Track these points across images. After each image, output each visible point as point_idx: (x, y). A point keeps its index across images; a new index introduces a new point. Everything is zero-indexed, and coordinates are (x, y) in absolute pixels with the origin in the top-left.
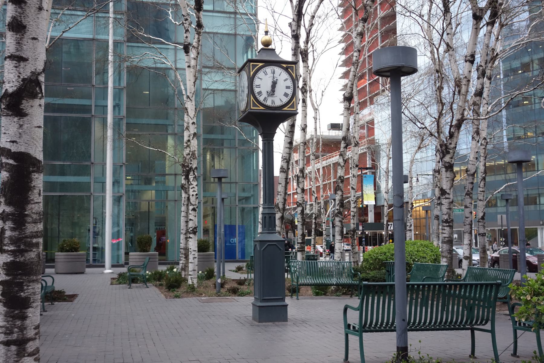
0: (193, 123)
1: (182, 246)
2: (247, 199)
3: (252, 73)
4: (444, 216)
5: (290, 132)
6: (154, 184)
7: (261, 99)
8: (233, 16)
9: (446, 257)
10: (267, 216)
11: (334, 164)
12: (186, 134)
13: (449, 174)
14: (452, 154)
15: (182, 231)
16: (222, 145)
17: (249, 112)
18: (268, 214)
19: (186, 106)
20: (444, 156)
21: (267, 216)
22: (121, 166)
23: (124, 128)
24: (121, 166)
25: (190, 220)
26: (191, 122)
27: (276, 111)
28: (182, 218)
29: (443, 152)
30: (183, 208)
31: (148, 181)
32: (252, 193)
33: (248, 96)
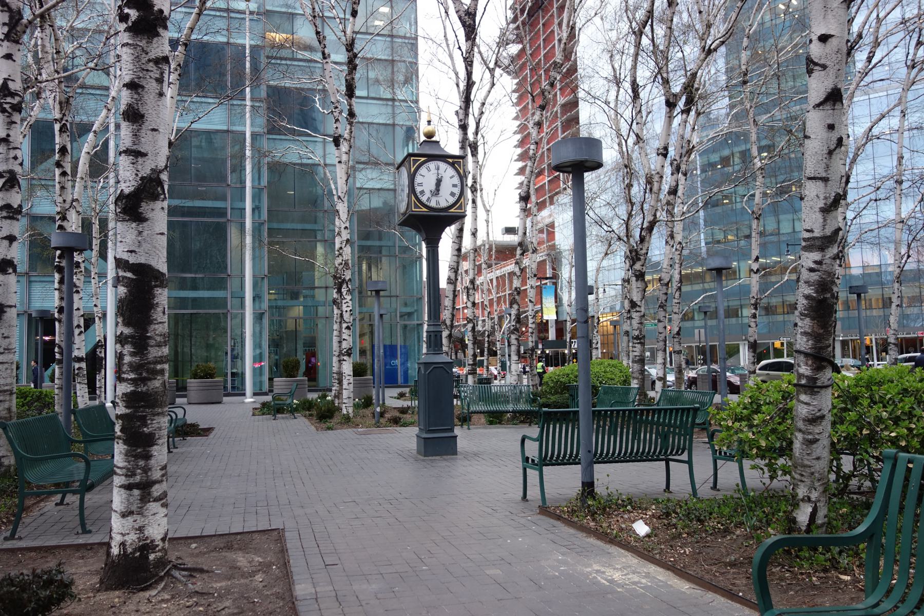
0: (346, 228)
1: (335, 369)
2: (410, 315)
3: (413, 169)
7: (424, 199)
9: (637, 378)
12: (338, 241)
13: (640, 284)
16: (380, 252)
20: (634, 263)
21: (432, 334)
22: (263, 278)
23: (266, 234)
24: (263, 278)
26: (343, 226)
28: (334, 338)
30: (336, 327)
31: (295, 296)
33: (409, 196)
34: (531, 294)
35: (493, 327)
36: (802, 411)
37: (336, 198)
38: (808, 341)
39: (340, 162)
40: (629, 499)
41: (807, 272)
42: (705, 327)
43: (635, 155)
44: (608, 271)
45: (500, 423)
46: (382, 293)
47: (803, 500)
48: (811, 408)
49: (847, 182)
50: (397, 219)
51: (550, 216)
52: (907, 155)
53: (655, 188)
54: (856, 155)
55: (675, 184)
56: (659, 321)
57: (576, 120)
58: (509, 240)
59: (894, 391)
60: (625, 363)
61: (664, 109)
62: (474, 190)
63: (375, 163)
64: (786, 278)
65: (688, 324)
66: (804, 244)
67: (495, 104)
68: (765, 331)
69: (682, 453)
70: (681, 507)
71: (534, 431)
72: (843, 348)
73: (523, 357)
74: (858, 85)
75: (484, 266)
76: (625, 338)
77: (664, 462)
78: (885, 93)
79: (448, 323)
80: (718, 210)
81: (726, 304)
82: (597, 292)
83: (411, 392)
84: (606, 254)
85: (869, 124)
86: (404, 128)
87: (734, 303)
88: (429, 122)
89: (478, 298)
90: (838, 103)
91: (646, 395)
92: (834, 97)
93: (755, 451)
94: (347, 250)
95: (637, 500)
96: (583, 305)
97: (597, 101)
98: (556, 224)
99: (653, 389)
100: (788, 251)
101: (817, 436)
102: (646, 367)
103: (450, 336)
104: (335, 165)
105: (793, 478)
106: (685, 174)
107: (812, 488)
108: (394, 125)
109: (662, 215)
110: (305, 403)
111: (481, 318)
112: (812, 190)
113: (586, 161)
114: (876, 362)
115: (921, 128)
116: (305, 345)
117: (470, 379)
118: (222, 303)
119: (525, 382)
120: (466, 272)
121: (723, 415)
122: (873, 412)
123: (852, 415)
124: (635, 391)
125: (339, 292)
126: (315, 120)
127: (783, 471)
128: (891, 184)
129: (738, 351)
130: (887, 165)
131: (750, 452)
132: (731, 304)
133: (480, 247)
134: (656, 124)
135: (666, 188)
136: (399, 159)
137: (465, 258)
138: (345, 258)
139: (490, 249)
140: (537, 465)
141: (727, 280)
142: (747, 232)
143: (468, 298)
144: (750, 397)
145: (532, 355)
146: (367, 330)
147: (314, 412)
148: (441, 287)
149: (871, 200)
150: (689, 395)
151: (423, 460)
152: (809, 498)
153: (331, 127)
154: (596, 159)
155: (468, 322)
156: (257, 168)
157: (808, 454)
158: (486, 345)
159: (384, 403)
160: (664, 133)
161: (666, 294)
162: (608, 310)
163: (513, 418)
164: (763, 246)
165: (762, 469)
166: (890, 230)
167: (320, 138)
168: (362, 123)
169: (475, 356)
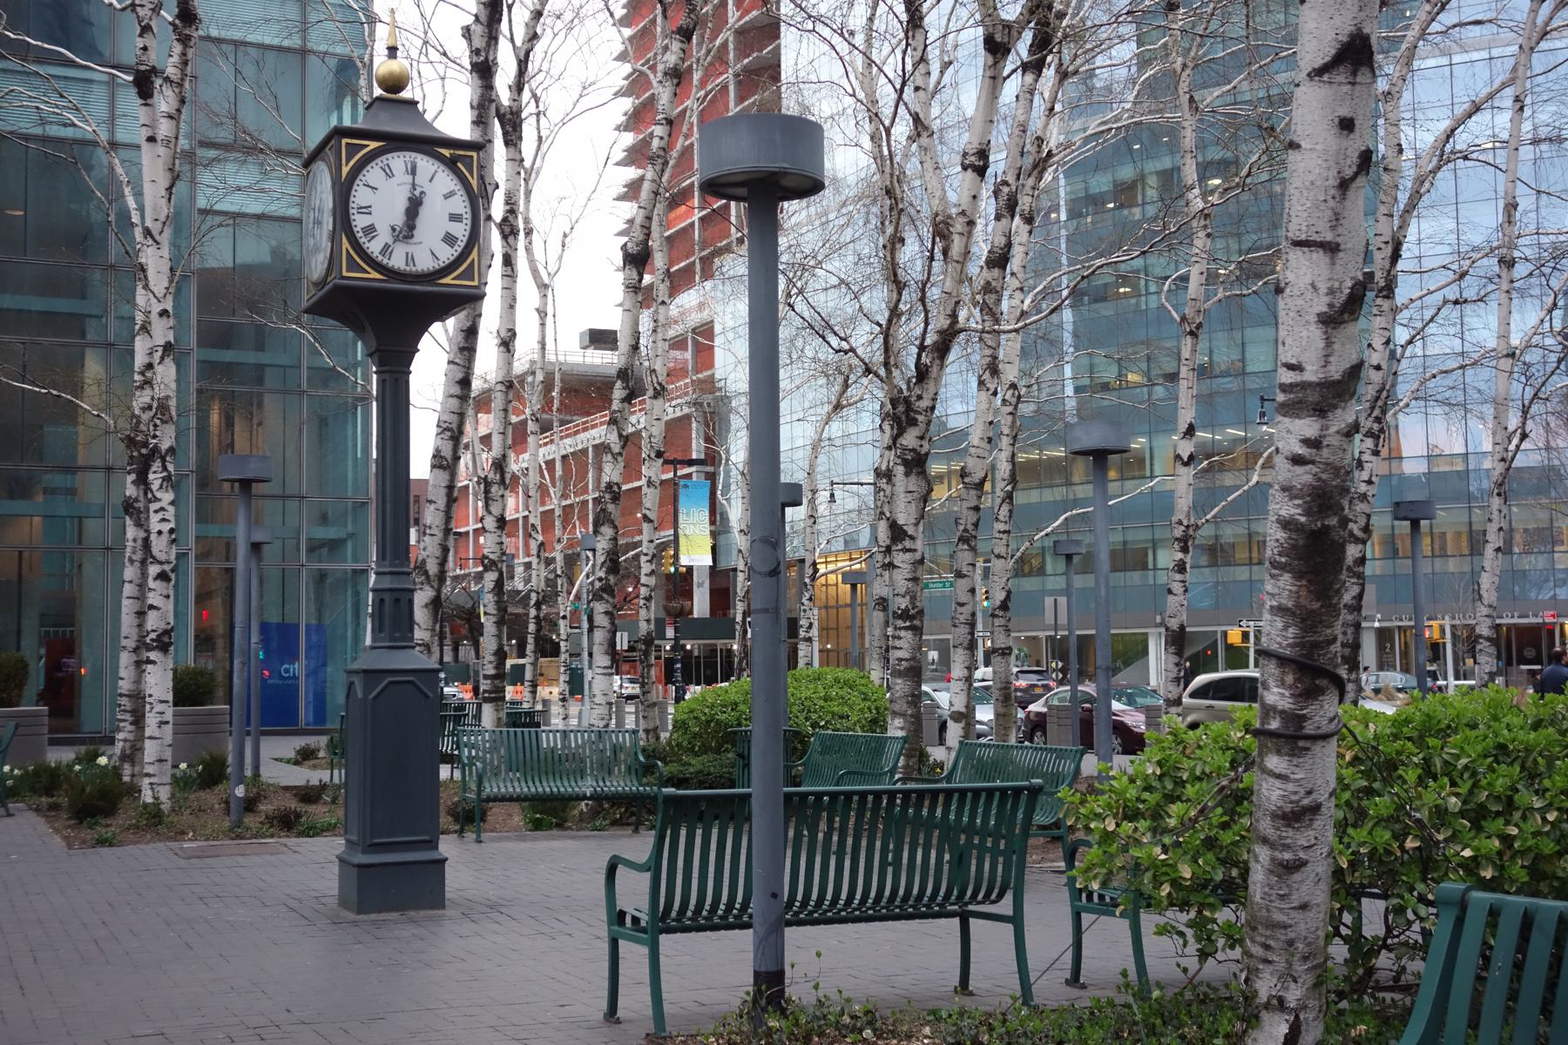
0: (164, 313)
1: (125, 686)
2: (335, 546)
3: (345, 170)
4: (899, 599)
5: (462, 349)
6: (40, 498)
7: (374, 248)
9: (903, 715)
10: (387, 597)
12: (141, 346)
13: (914, 483)
14: (922, 426)
15: (124, 642)
16: (260, 381)
17: (337, 288)
21: (387, 597)
26: (156, 308)
27: (418, 288)
28: (125, 602)
32: (350, 528)
33: (334, 237)
34: (650, 498)
35: (551, 583)
36: (1271, 794)
37: (138, 233)
38: (1286, 628)
39: (151, 139)
40: (867, 1012)
41: (1288, 466)
42: (1067, 592)
43: (912, 167)
44: (833, 447)
45: (560, 826)
46: (257, 488)
47: (1267, 1006)
48: (1291, 787)
49: (1396, 256)
50: (306, 298)
51: (701, 306)
52: (1526, 202)
53: (956, 249)
54: (1416, 196)
55: (1003, 241)
56: (959, 575)
57: (770, 71)
58: (598, 361)
59: (1474, 751)
60: (875, 676)
61: (982, 57)
62: (509, 231)
63: (248, 148)
64: (1255, 479)
65: (1030, 584)
66: (1281, 397)
67: (568, 16)
68: (1206, 603)
69: (1001, 896)
70: (991, 1029)
71: (639, 846)
72: (1381, 648)
73: (627, 660)
74: (1423, 34)
75: (532, 426)
76: (878, 616)
77: (956, 921)
78: (1485, 55)
79: (432, 568)
80: (1106, 309)
81: (1117, 537)
82: (812, 501)
83: (332, 746)
84: (838, 407)
85: (1445, 124)
86: (332, 62)
87: (1138, 536)
88: (392, 51)
89: (513, 507)
90: (1364, 70)
91: (923, 756)
92: (1355, 55)
93: (1166, 889)
94: (166, 373)
95: (887, 1013)
96: (768, 532)
97: (820, 27)
98: (718, 328)
99: (942, 742)
100: (1263, 415)
101: (1302, 855)
102: (925, 688)
103: (436, 604)
104: (138, 147)
105: (1247, 953)
106: (1029, 220)
107: (1289, 976)
108: (303, 52)
109: (970, 316)
110: (36, 773)
111: (522, 559)
112: (1304, 275)
113: (783, 173)
114: (1452, 682)
115: (1559, 140)
117: (488, 715)
119: (630, 722)
120: (486, 440)
121: (1096, 805)
122: (1430, 797)
123: (1381, 805)
124: (897, 747)
125: (142, 481)
126: (91, 24)
127: (1229, 937)
128: (1491, 265)
129: (1145, 652)
130: (1483, 223)
131: (1154, 893)
132: (1130, 536)
133: (522, 379)
134: (963, 94)
135: (981, 249)
136: (315, 138)
137: (483, 403)
138: (159, 392)
139: (548, 385)
140: (644, 931)
141: (1122, 479)
142: (1170, 368)
143: (487, 506)
144: (1159, 763)
145: (646, 653)
146: (219, 585)
147: (64, 801)
148: (413, 476)
149: (1445, 302)
150: (1026, 757)
151: (355, 923)
152: (1281, 1000)
153: (130, 46)
154: (810, 171)
155: (486, 569)
157: (1282, 897)
158: (532, 627)
159: (257, 774)
160: (980, 118)
161: (977, 509)
162: (839, 545)
163: (595, 813)
164: (1206, 401)
165: (1181, 934)
166: (1485, 373)
167: (100, 73)
168: (218, 41)
169: (501, 655)
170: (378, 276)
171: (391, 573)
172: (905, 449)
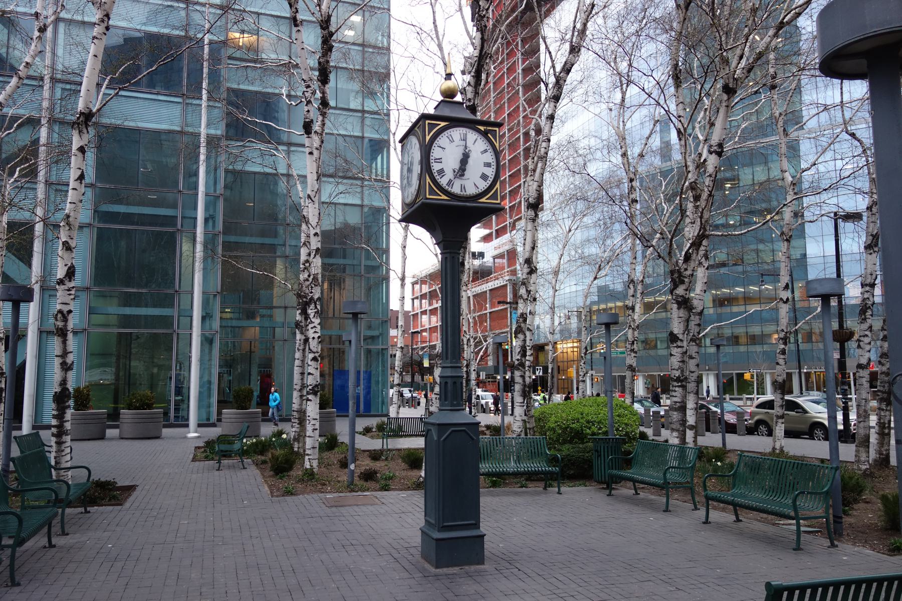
0: (316, 234)
1: (295, 407)
2: (373, 338)
3: (428, 138)
4: (675, 372)
6: (258, 320)
7: (443, 182)
8: (360, 114)
9: (678, 430)
10: (449, 381)
11: (490, 290)
12: (304, 252)
13: (683, 313)
14: (687, 284)
15: (295, 387)
16: (344, 272)
17: (423, 204)
18: (451, 377)
19: (305, 214)
20: (675, 286)
21: (449, 381)
22: (215, 296)
25: (309, 374)
26: (312, 232)
28: (296, 368)
29: (673, 280)
30: (298, 355)
31: (251, 315)
33: (421, 177)
84: (595, 278)
116: (260, 366)
118: (166, 321)
138: (313, 271)
156: (212, 170)
170: (446, 198)
171: (451, 367)
172: (678, 296)
